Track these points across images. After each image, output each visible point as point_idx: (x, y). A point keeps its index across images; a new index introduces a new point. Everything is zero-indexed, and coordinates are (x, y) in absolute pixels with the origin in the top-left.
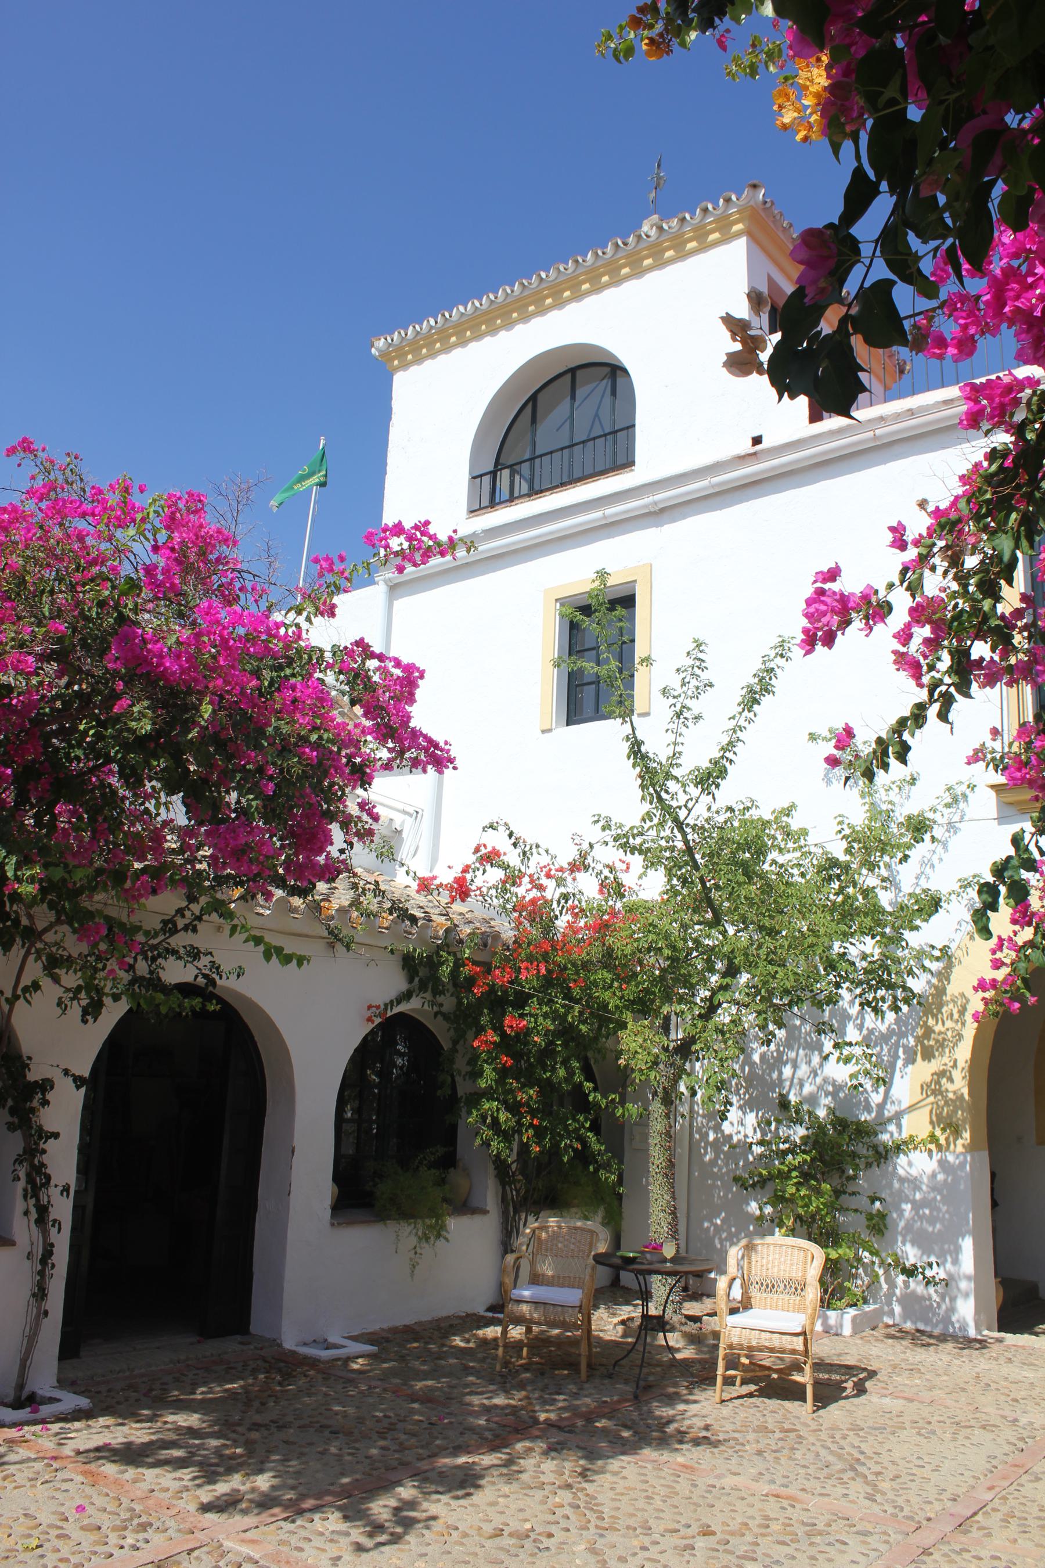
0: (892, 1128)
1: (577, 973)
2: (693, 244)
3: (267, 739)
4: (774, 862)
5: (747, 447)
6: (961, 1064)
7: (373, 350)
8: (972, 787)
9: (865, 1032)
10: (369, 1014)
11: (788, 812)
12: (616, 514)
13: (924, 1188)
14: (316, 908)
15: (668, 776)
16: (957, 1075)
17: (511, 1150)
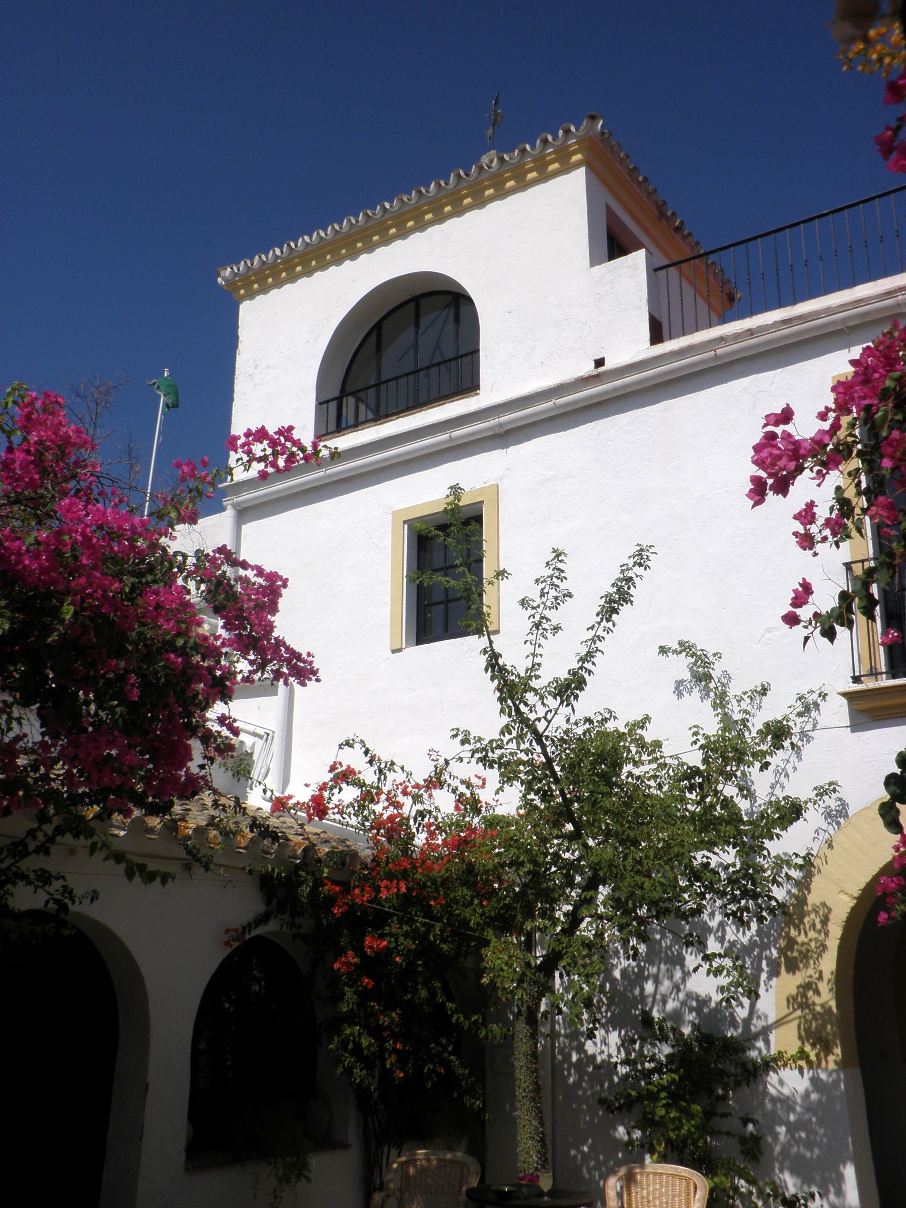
0: (760, 1044)
1: (437, 890)
2: (534, 175)
3: (131, 643)
4: (630, 774)
5: (588, 368)
6: (827, 975)
7: (219, 279)
8: (823, 696)
9: (726, 944)
10: (226, 938)
11: (643, 723)
12: (462, 437)
13: (798, 1109)
14: (172, 827)
15: (528, 688)
16: (824, 987)
17: (374, 1077)
